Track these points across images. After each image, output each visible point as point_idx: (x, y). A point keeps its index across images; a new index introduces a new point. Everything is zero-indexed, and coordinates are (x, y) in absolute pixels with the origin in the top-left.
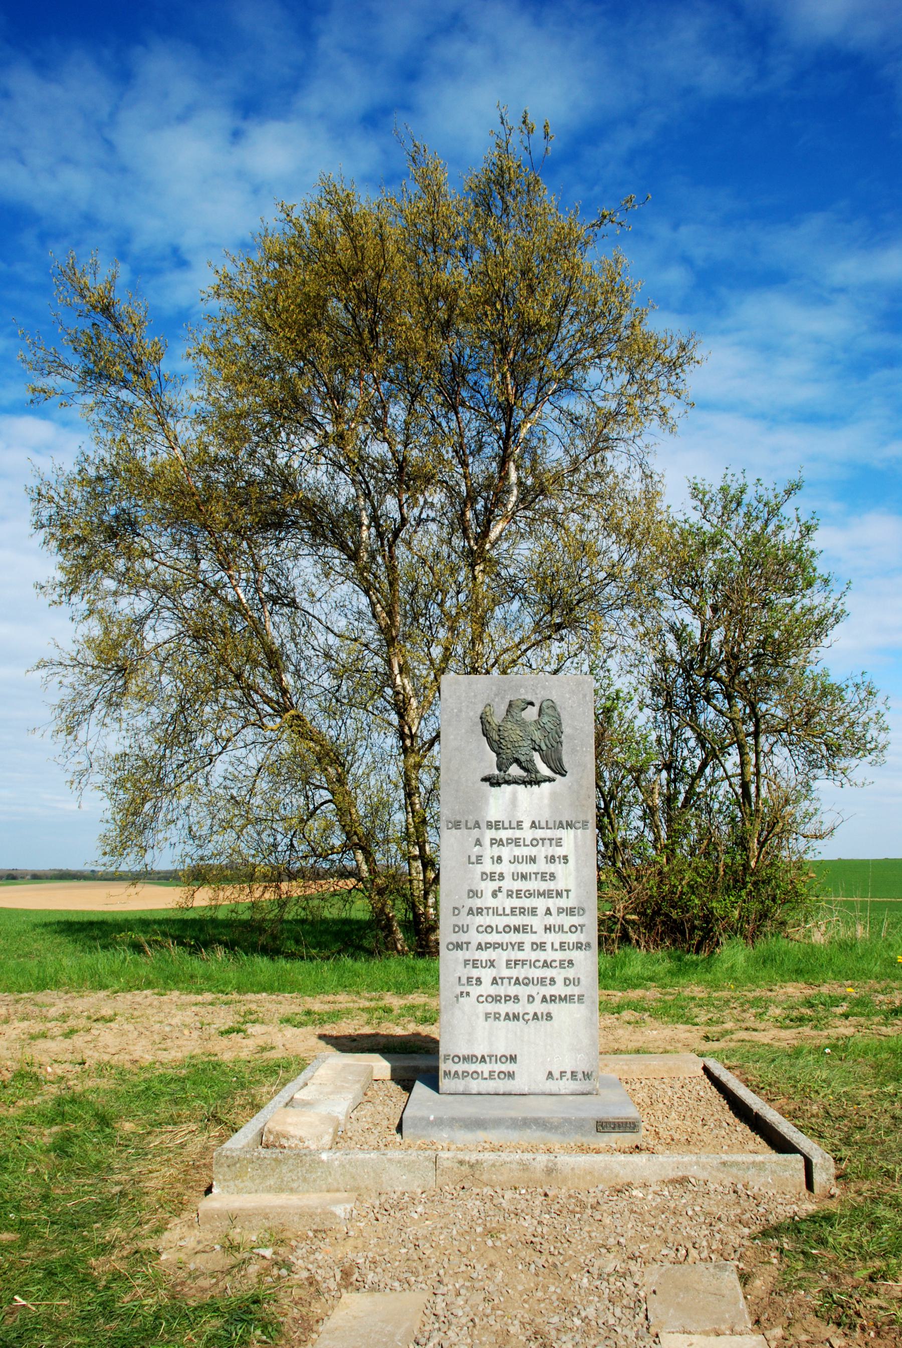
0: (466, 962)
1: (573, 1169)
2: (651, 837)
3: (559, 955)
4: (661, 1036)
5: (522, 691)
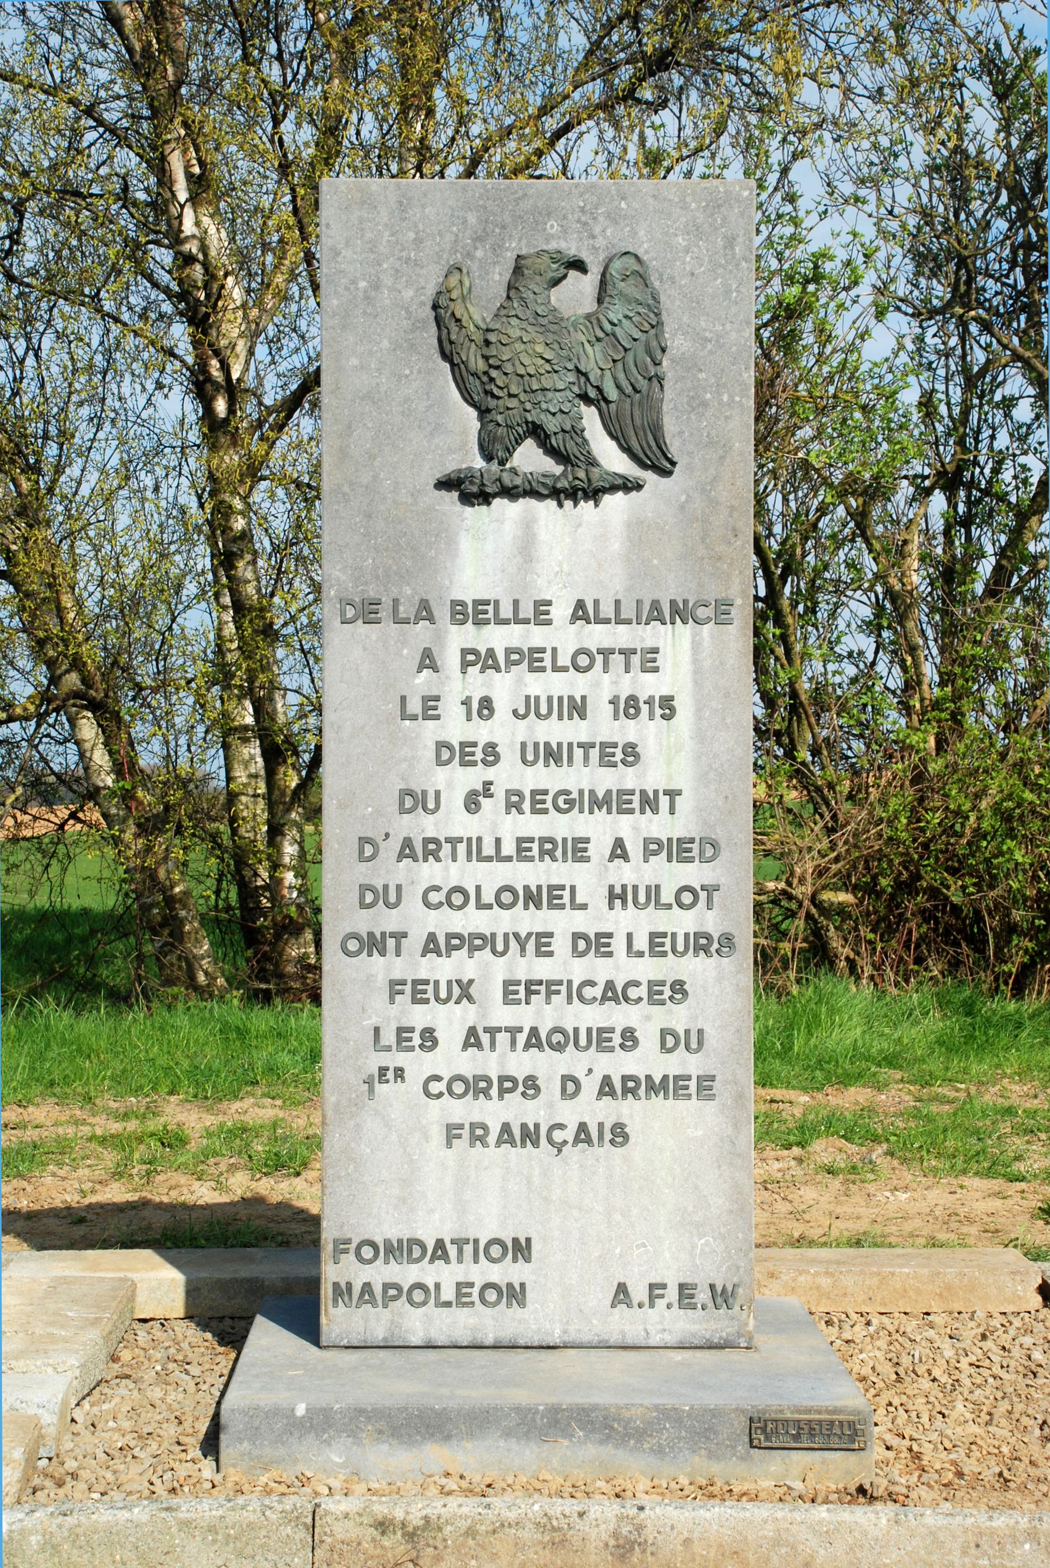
0: (395, 987)
1: (687, 1542)
2: (895, 680)
3: (647, 969)
4: (923, 1206)
5: (553, 226)
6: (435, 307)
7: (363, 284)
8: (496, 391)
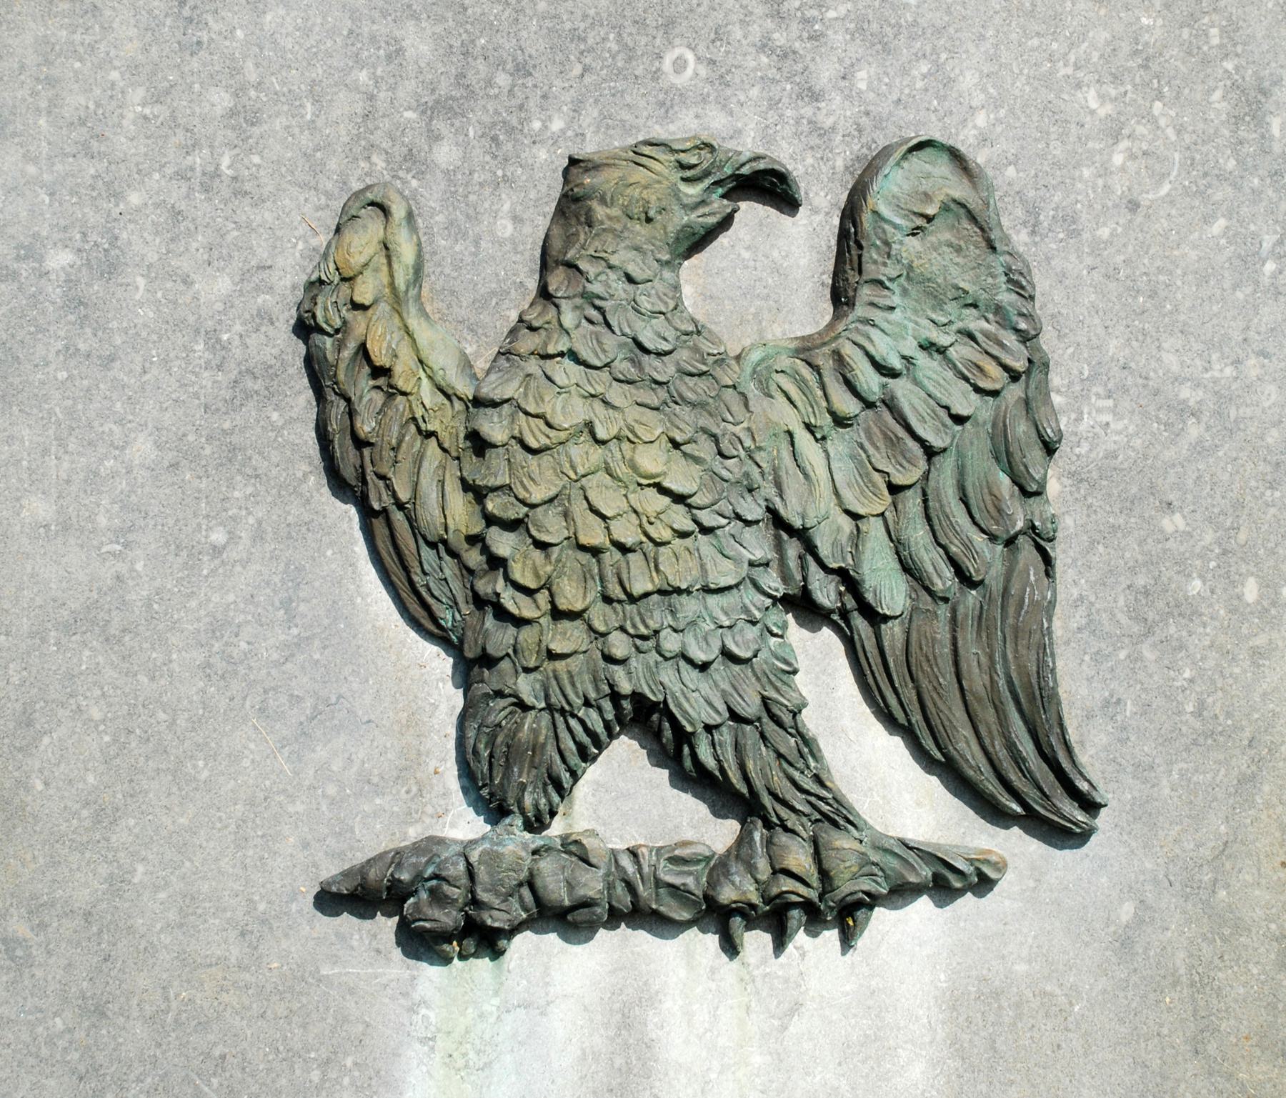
5: (683, 65)
6: (305, 328)
7: (59, 260)
8: (510, 600)
